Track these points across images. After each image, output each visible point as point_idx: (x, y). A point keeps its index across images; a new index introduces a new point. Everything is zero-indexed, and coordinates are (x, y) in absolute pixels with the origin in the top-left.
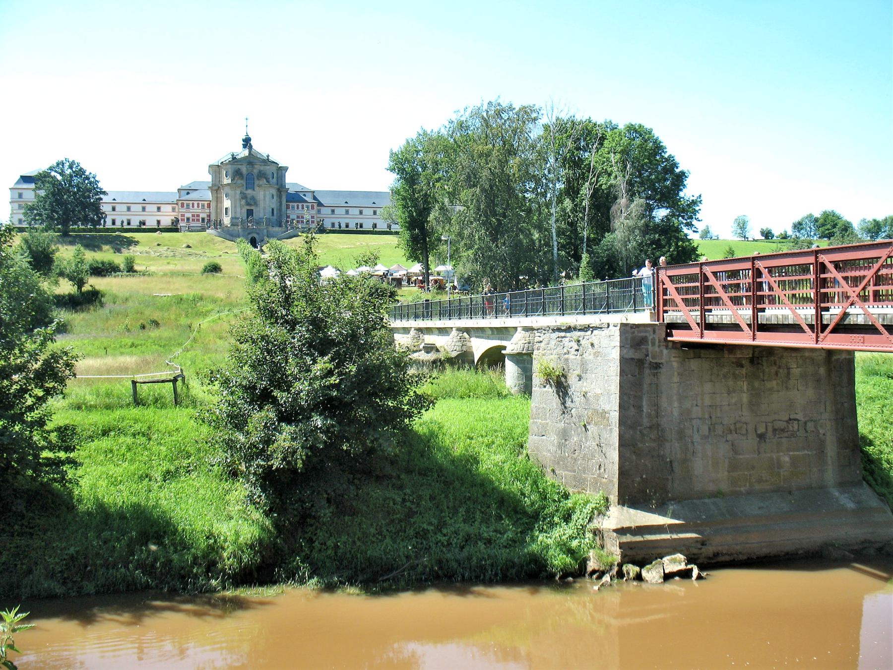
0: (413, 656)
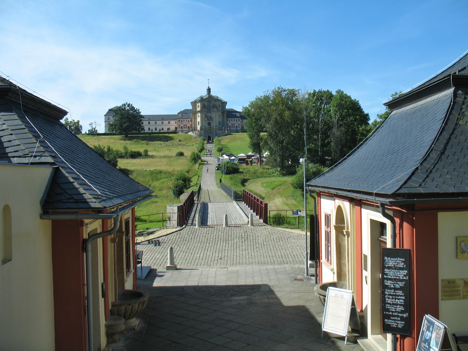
0: (342, 100)
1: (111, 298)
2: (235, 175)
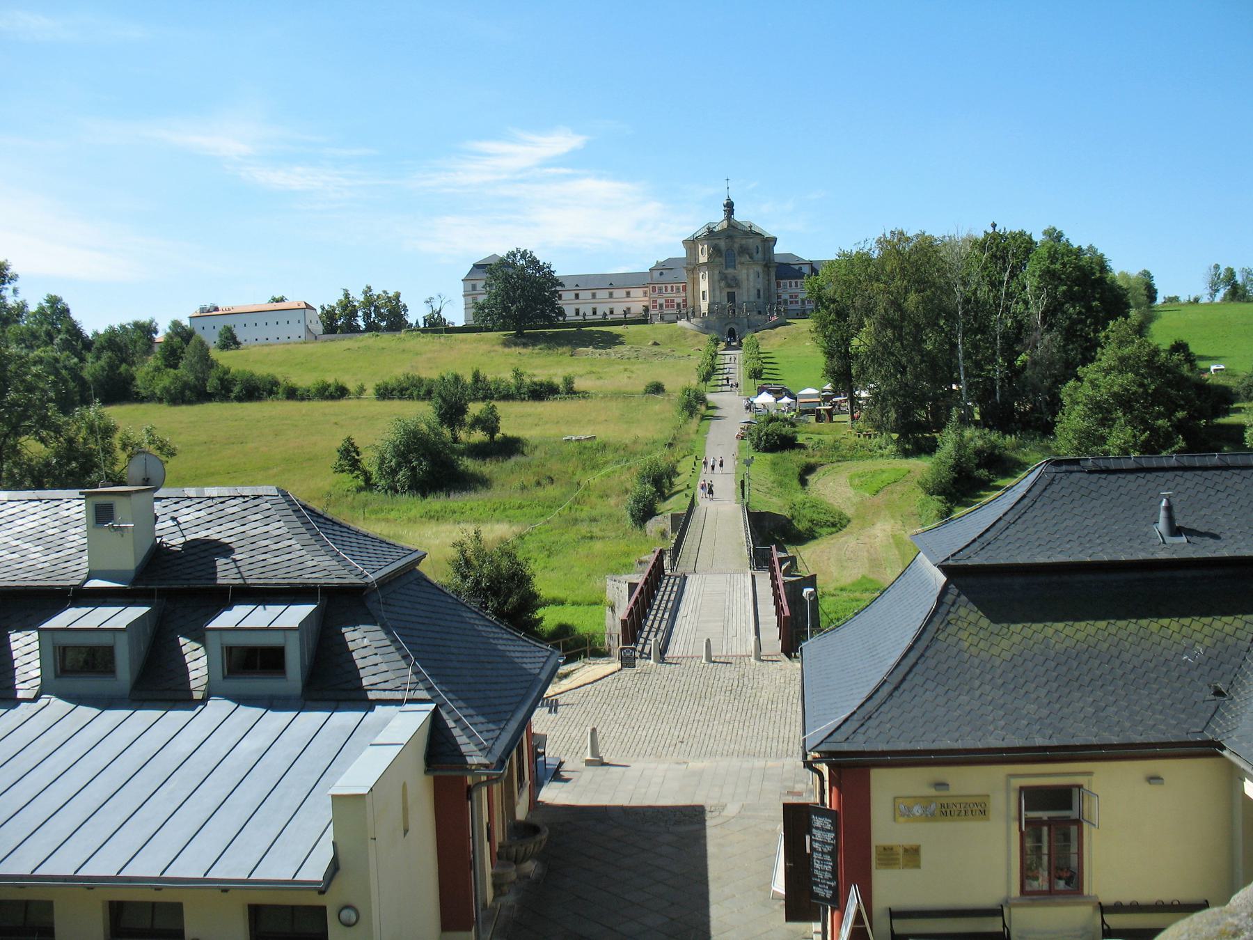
1: (498, 837)
2: (786, 454)
